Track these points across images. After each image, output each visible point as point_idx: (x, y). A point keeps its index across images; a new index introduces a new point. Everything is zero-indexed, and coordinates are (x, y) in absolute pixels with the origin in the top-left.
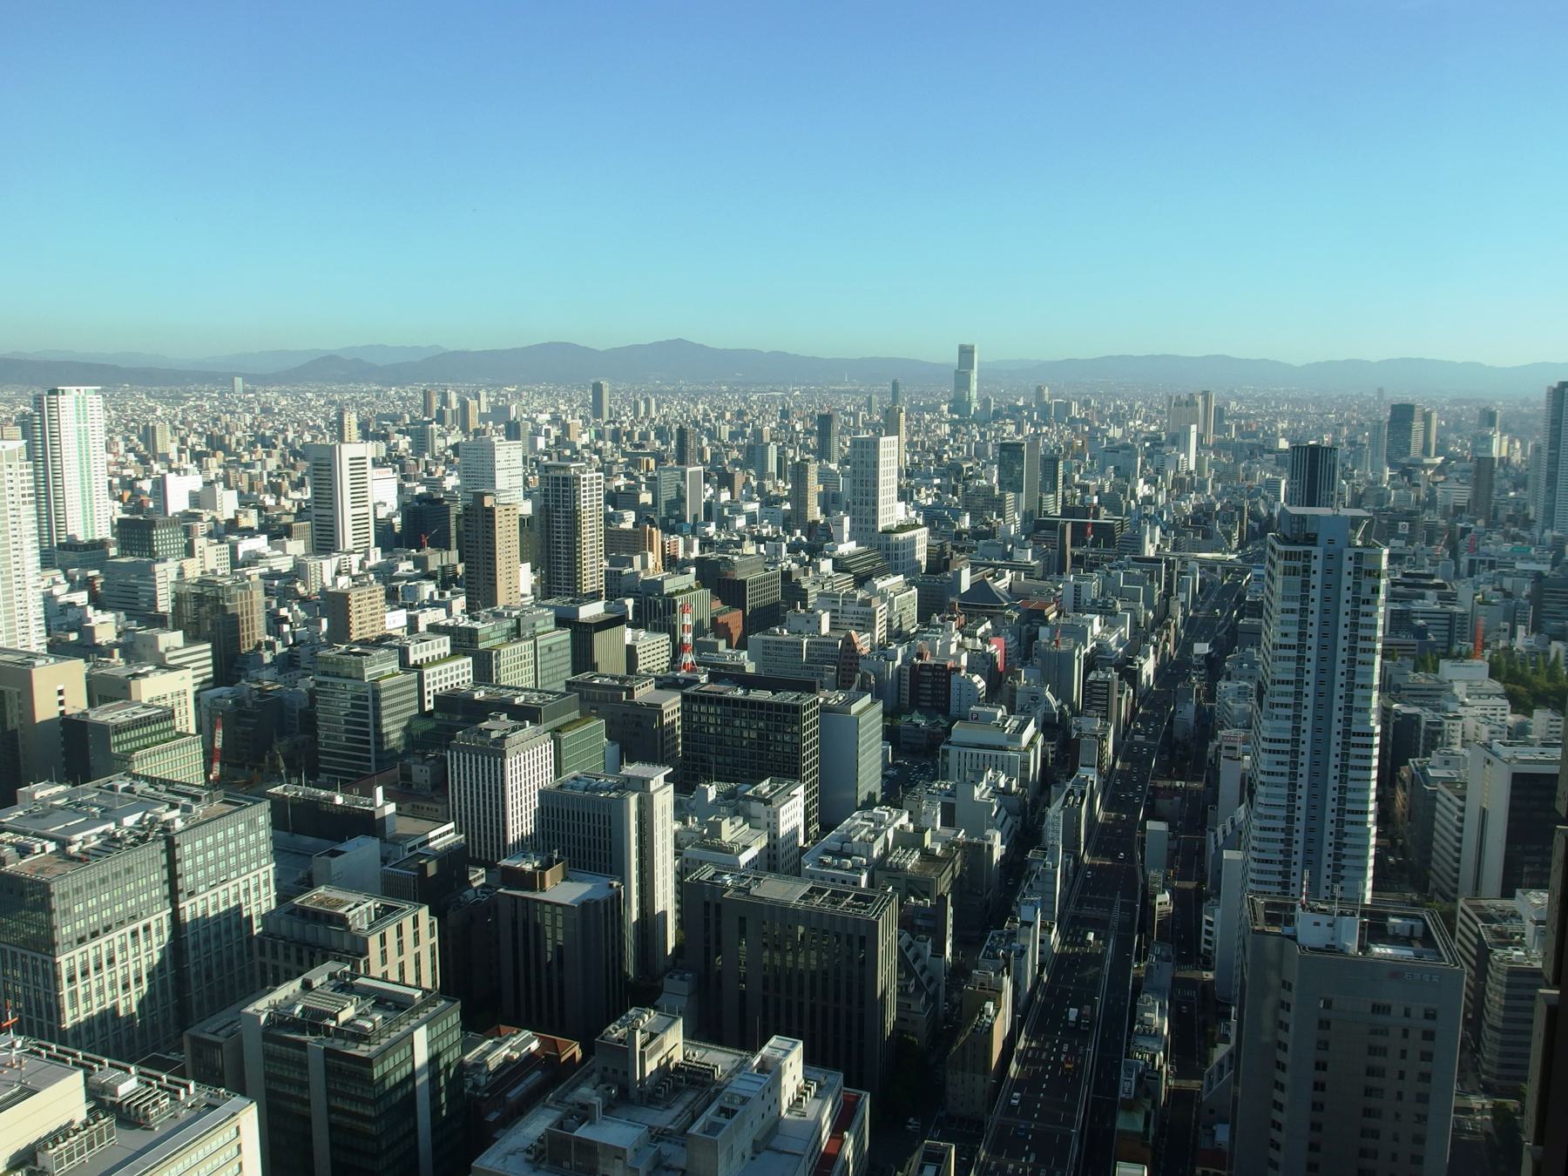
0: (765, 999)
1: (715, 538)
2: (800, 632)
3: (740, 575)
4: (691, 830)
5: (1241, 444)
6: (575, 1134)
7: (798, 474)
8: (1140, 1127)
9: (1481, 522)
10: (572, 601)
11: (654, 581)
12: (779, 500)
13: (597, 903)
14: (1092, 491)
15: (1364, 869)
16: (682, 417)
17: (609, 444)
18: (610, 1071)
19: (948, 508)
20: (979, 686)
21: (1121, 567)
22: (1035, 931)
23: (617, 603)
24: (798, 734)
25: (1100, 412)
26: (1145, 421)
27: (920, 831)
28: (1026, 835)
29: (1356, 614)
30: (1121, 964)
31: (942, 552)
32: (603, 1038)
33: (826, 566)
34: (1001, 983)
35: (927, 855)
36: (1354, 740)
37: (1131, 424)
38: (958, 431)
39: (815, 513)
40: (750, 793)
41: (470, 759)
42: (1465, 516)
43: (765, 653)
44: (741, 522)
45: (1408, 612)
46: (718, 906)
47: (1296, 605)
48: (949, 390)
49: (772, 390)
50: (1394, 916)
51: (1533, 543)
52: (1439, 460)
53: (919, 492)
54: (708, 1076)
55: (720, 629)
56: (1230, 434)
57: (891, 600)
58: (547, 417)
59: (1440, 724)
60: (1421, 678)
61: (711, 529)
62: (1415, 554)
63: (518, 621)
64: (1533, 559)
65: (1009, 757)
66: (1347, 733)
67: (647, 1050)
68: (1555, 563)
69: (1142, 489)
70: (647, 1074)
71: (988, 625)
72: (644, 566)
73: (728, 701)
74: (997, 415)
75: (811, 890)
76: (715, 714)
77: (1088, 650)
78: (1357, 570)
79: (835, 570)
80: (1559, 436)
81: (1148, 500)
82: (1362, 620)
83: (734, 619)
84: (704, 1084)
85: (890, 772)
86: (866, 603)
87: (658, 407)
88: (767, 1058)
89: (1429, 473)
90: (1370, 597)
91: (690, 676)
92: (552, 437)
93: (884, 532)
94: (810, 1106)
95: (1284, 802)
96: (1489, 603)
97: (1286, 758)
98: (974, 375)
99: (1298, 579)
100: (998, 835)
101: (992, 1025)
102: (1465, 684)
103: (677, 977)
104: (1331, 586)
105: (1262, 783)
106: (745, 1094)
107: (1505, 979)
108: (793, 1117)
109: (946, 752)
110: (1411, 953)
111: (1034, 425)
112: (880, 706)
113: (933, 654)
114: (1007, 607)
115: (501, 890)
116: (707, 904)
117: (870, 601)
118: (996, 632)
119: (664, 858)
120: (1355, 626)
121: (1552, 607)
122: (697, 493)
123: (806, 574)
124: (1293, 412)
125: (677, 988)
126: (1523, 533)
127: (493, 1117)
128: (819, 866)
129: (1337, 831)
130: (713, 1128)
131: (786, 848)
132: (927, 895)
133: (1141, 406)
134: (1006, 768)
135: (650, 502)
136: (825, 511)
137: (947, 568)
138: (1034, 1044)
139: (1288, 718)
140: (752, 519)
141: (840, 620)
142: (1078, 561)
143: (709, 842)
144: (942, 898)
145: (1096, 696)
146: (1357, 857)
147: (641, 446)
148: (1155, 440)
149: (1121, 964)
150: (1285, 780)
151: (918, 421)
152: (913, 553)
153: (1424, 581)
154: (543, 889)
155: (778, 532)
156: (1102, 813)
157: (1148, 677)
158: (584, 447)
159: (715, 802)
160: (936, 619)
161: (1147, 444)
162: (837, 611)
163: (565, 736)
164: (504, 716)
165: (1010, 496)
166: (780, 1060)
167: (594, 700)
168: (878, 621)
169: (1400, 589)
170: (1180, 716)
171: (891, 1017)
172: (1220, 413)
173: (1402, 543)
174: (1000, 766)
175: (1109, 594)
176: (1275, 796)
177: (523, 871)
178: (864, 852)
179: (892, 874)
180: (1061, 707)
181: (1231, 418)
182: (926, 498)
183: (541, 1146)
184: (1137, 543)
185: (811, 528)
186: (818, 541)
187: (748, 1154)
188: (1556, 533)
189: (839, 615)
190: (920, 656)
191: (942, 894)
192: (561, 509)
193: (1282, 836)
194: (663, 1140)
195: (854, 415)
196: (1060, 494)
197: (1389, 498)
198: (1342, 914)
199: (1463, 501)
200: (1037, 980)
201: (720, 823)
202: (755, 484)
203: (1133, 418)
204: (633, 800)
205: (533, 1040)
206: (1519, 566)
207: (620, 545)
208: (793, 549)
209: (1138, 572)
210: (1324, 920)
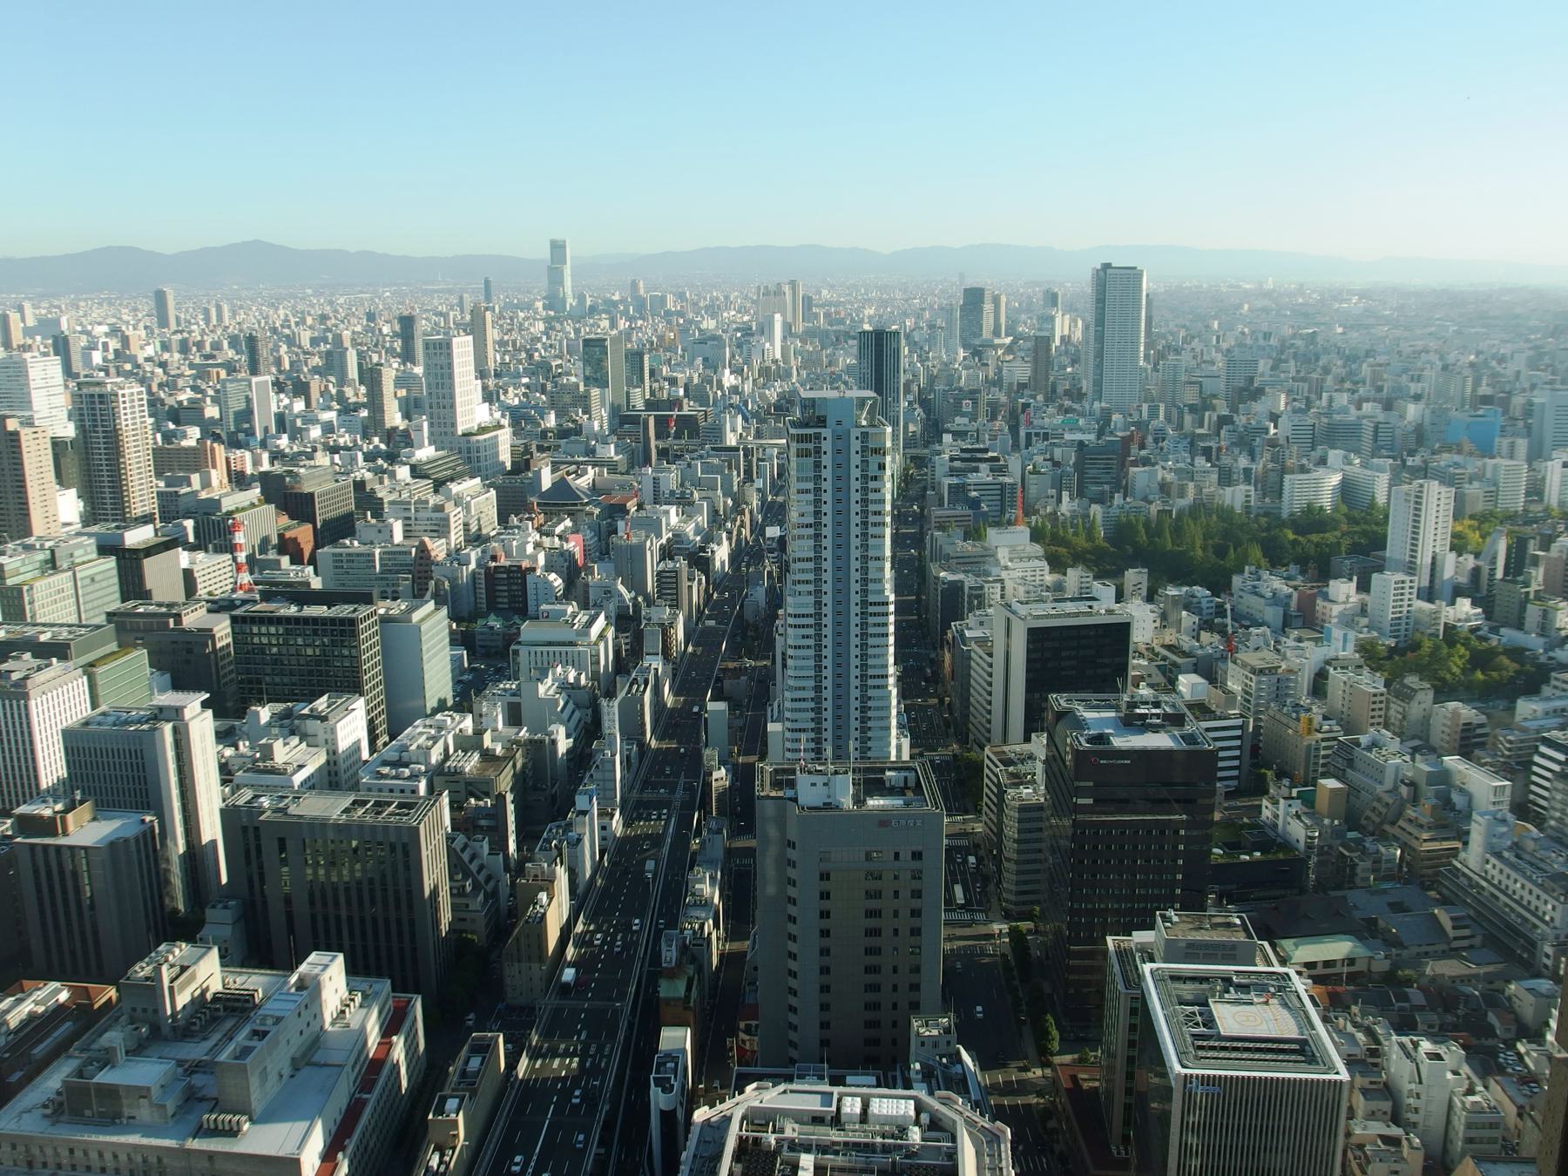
0: (313, 917)
1: (287, 450)
2: (372, 543)
3: (307, 488)
4: (242, 756)
5: (827, 331)
6: (94, 1080)
7: (371, 377)
8: (682, 992)
9: (1040, 398)
10: (118, 527)
11: (211, 500)
12: (357, 407)
13: (126, 841)
14: (681, 383)
15: (888, 728)
16: (259, 323)
17: (177, 356)
18: (139, 1010)
19: (535, 407)
20: (556, 584)
21: (701, 457)
22: (592, 819)
23: (176, 526)
24: (357, 647)
25: (695, 304)
26: (739, 312)
27: (479, 733)
28: (589, 730)
29: (865, 490)
30: (681, 841)
31: (527, 451)
32: (128, 979)
33: (403, 473)
34: (554, 872)
35: (487, 756)
36: (871, 609)
37: (725, 314)
38: (552, 328)
39: (394, 418)
40: (306, 711)
41: (11, 706)
42: (1027, 392)
43: (336, 567)
44: (315, 432)
45: (964, 485)
46: (256, 829)
47: (810, 486)
48: (544, 283)
49: (361, 292)
50: (890, 769)
51: (1082, 415)
52: (1008, 340)
53: (506, 392)
54: (247, 1001)
55: (287, 546)
56: (819, 322)
57: (468, 503)
58: (105, 329)
59: (982, 588)
60: (969, 547)
61: (284, 442)
62: (978, 431)
63: (53, 552)
64: (1081, 430)
65: (579, 653)
66: (864, 603)
67: (176, 984)
68: (1100, 434)
69: (729, 379)
70: (179, 1007)
71: (568, 523)
72: (206, 484)
73: (280, 621)
74: (593, 310)
75: (354, 802)
76: (277, 634)
77: (664, 541)
78: (864, 449)
79: (413, 477)
80: (1103, 314)
81: (735, 390)
82: (872, 496)
83: (304, 534)
84: (244, 1010)
85: (465, 677)
86: (439, 508)
87: (234, 314)
88: (305, 975)
89: (1000, 352)
90: (878, 473)
91: (247, 596)
92: (111, 350)
93: (464, 435)
94: (354, 1017)
95: (812, 673)
96: (1039, 473)
97: (811, 631)
98: (567, 272)
99: (811, 460)
100: (562, 730)
101: (544, 914)
102: (1007, 550)
103: (220, 906)
104: (841, 466)
105: (791, 657)
106: (278, 1014)
107: (1017, 815)
108: (336, 1028)
109: (516, 653)
110: (901, 802)
111: (631, 319)
112: (444, 611)
113: (508, 555)
114: (587, 504)
115: (18, 840)
116: (245, 829)
117: (443, 506)
118: (575, 530)
119: (208, 789)
120: (865, 502)
121: (1092, 472)
122: (265, 402)
123: (381, 482)
124: (880, 299)
125: (220, 919)
126: (1076, 406)
127: (15, 1077)
128: (377, 778)
129: (862, 696)
130: (245, 1052)
131: (348, 763)
132: (487, 795)
133: (736, 297)
134: (576, 663)
135: (217, 416)
136: (407, 416)
137: (528, 468)
138: (592, 928)
139: (810, 593)
140: (328, 428)
141: (413, 528)
142: (663, 453)
143: (263, 767)
144: (501, 798)
145: (669, 586)
146: (882, 718)
147: (213, 357)
148: (747, 331)
149: (681, 841)
150: (811, 652)
151: (511, 319)
152: (497, 454)
153: (979, 455)
154: (65, 833)
155: (355, 441)
156: (671, 697)
157: (723, 563)
158: (148, 359)
159: (269, 724)
160: (514, 520)
161: (739, 335)
162: (409, 518)
163: (99, 670)
164: (27, 656)
165: (595, 392)
166: (317, 975)
167: (138, 630)
168: (453, 526)
169: (957, 464)
170: (752, 598)
171: (446, 917)
172: (808, 302)
173: (965, 420)
174: (570, 662)
175: (687, 484)
176: (802, 668)
177: (41, 817)
178: (422, 759)
179: (452, 779)
180: (635, 599)
181: (822, 306)
182: (513, 398)
183: (60, 1098)
184: (717, 432)
185: (390, 435)
186: (398, 443)
187: (287, 1072)
188: (1103, 405)
189: (412, 522)
190: (494, 558)
191: (500, 794)
192: (100, 429)
193: (812, 705)
194: (197, 1072)
195: (445, 316)
196: (647, 388)
197: (960, 378)
198: (836, 773)
199: (1024, 380)
200: (597, 867)
201: (271, 745)
202: (334, 391)
203: (728, 309)
204: (168, 729)
205: (61, 991)
206: (1068, 436)
207: (169, 461)
208: (369, 457)
209: (716, 461)
210: (820, 780)
